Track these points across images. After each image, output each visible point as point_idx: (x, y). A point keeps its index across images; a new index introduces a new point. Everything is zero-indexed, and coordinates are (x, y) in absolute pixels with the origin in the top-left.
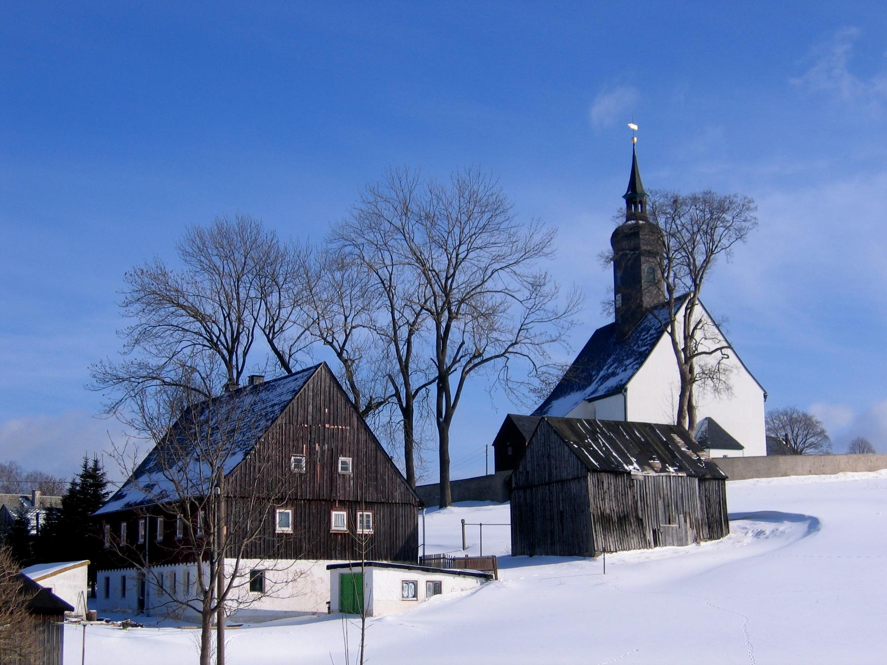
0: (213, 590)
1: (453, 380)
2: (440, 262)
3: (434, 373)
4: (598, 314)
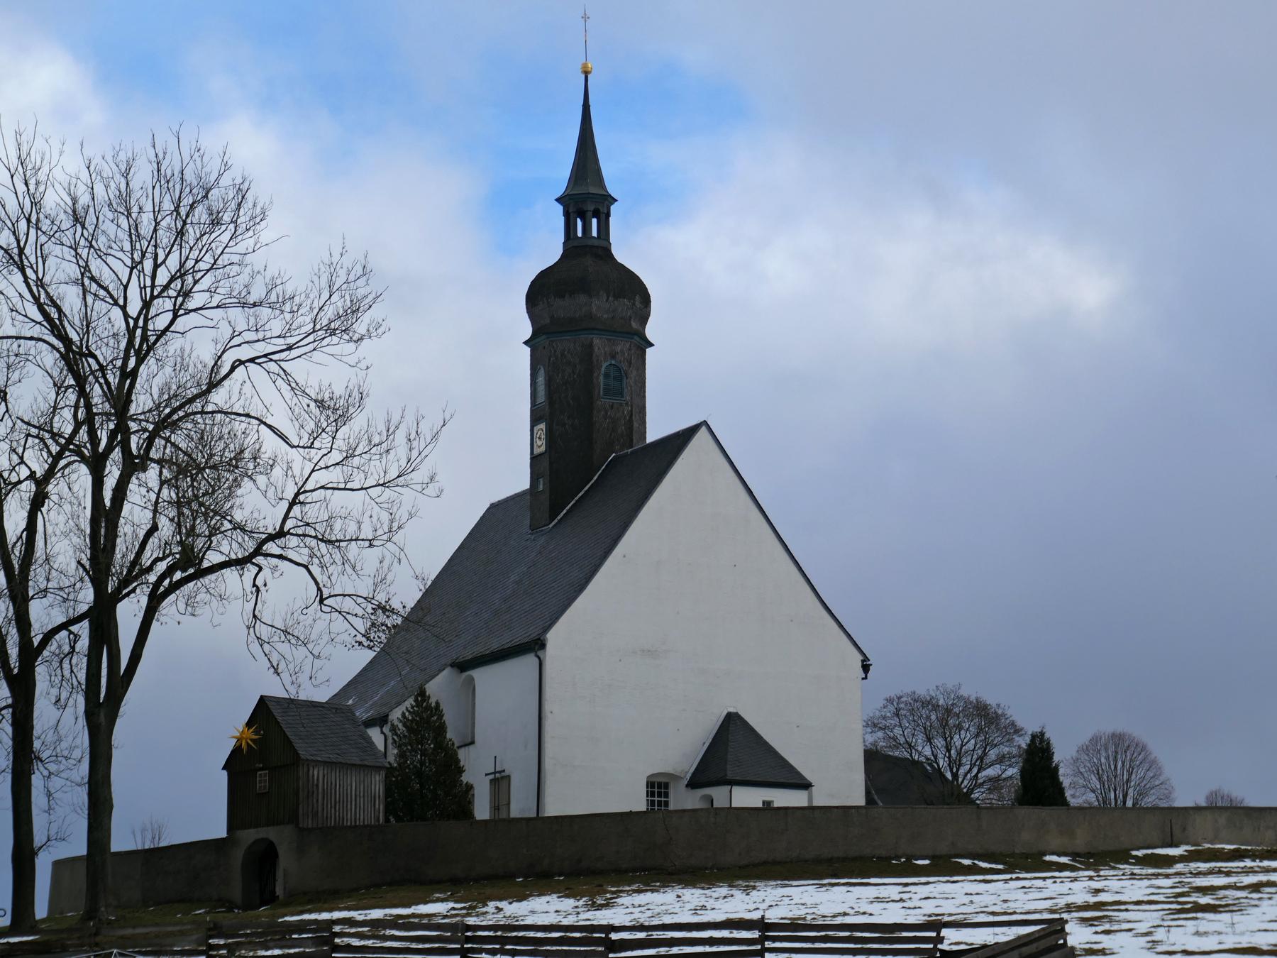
0: (175, 924)
1: (129, 613)
2: (107, 345)
3: (87, 595)
4: (496, 455)
